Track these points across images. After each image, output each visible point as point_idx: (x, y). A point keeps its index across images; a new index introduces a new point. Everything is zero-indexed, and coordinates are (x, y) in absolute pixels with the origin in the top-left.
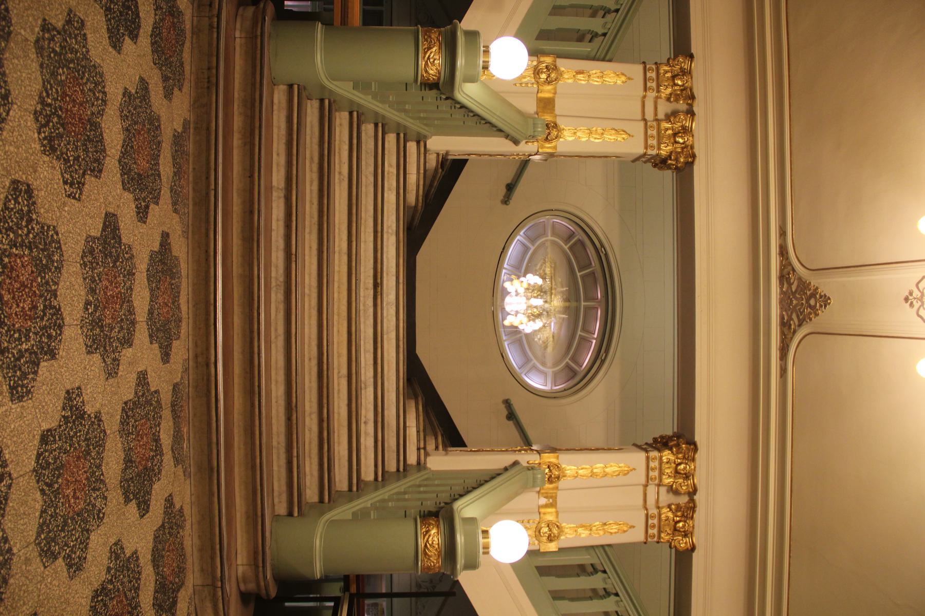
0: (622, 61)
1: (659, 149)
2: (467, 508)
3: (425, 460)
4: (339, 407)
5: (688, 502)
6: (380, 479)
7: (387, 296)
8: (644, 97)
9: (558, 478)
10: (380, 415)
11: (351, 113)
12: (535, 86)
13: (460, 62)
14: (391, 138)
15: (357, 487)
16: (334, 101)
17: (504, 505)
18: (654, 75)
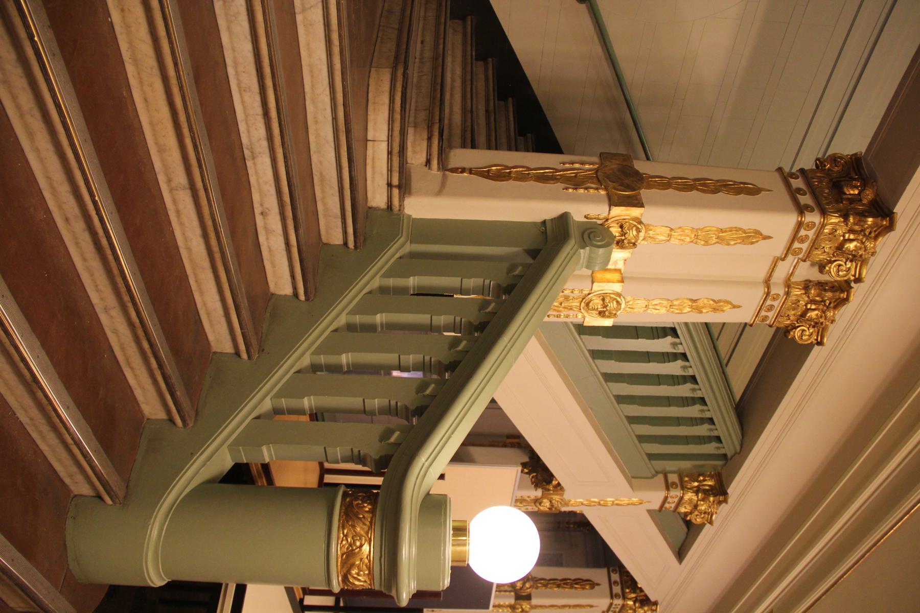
3: (401, 205)
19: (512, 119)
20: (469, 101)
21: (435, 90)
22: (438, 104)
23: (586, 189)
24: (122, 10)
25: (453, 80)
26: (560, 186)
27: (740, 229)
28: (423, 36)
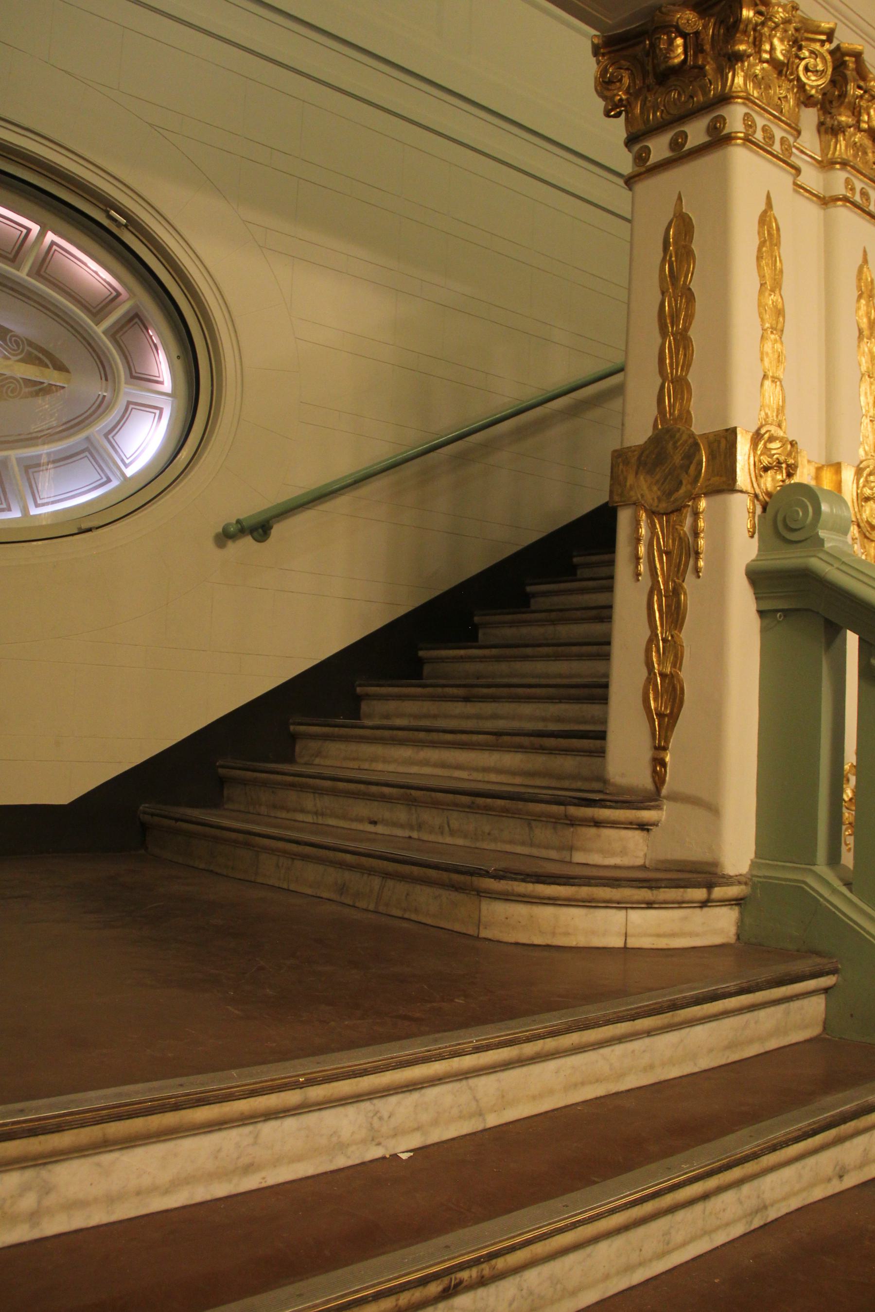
7: (342, 1146)
19: (462, 652)
20: (475, 738)
21: (487, 808)
22: (520, 805)
23: (696, 534)
25: (426, 763)
26: (689, 582)
27: (759, 250)
28: (360, 820)
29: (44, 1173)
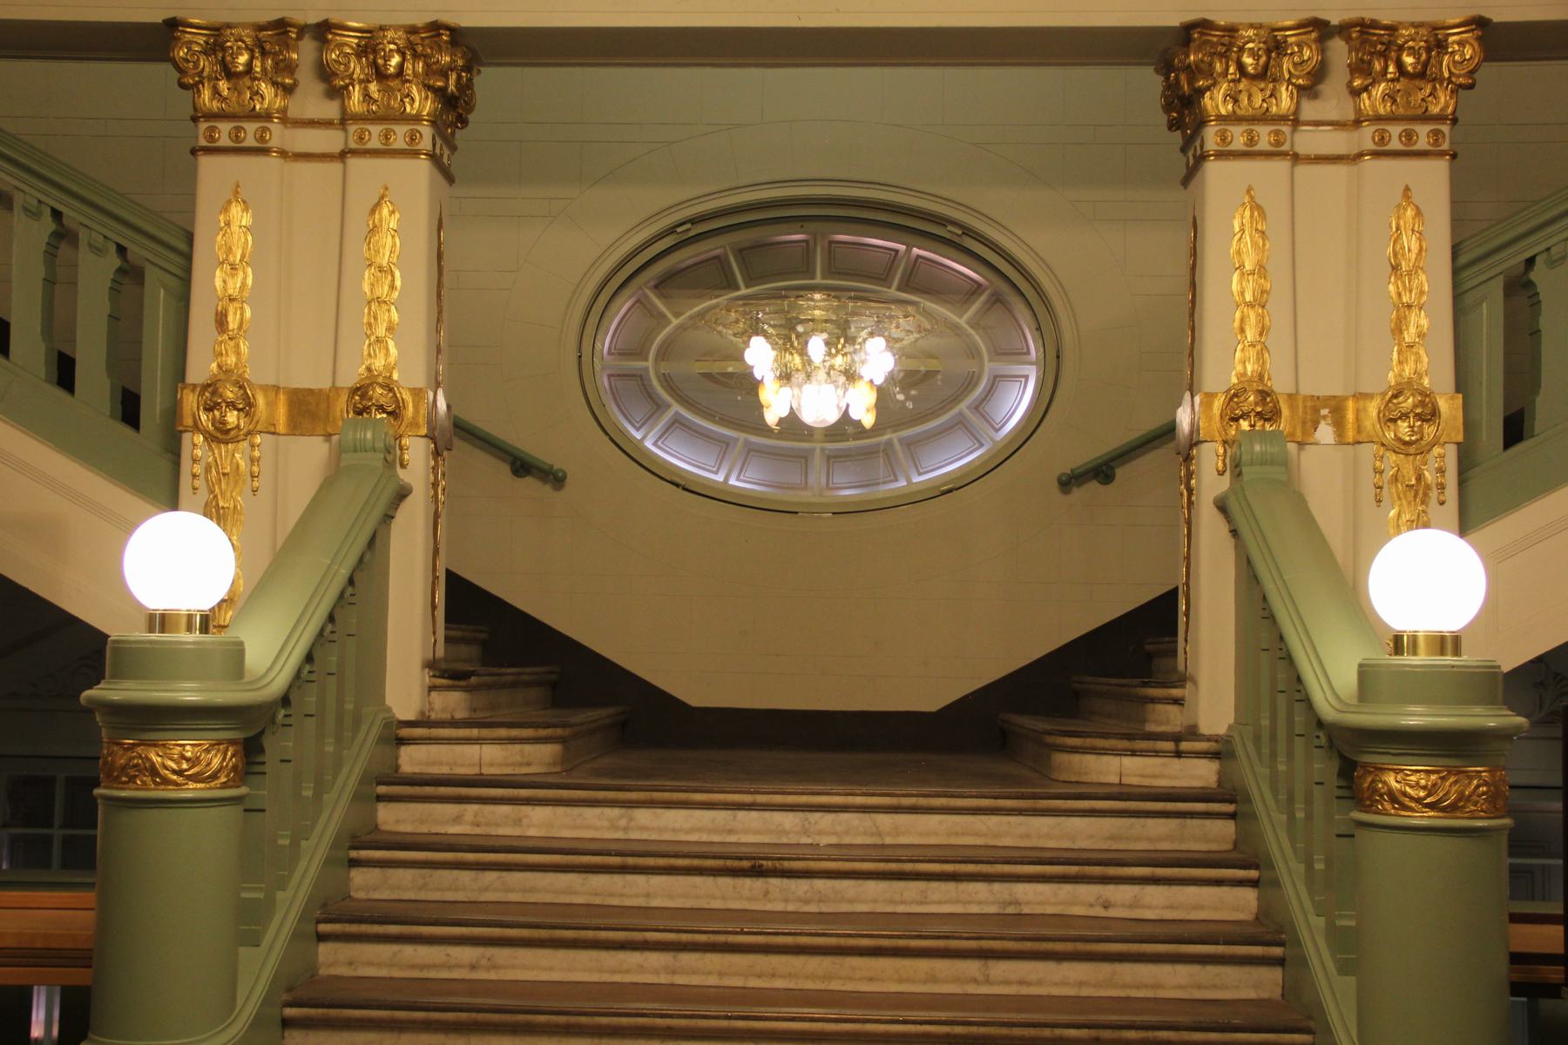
0: (190, 211)
1: (417, 119)
2: (1334, 674)
3: (1209, 739)
4: (1064, 984)
5: (1348, 39)
6: (1253, 874)
7: (786, 833)
8: (283, 154)
9: (1264, 394)
10: (1088, 870)
11: (322, 938)
12: (258, 440)
13: (189, 693)
14: (395, 818)
15: (1266, 938)
16: (290, 989)
17: (1335, 561)
18: (225, 128)
24: (774, 975)
29: (630, 811)
